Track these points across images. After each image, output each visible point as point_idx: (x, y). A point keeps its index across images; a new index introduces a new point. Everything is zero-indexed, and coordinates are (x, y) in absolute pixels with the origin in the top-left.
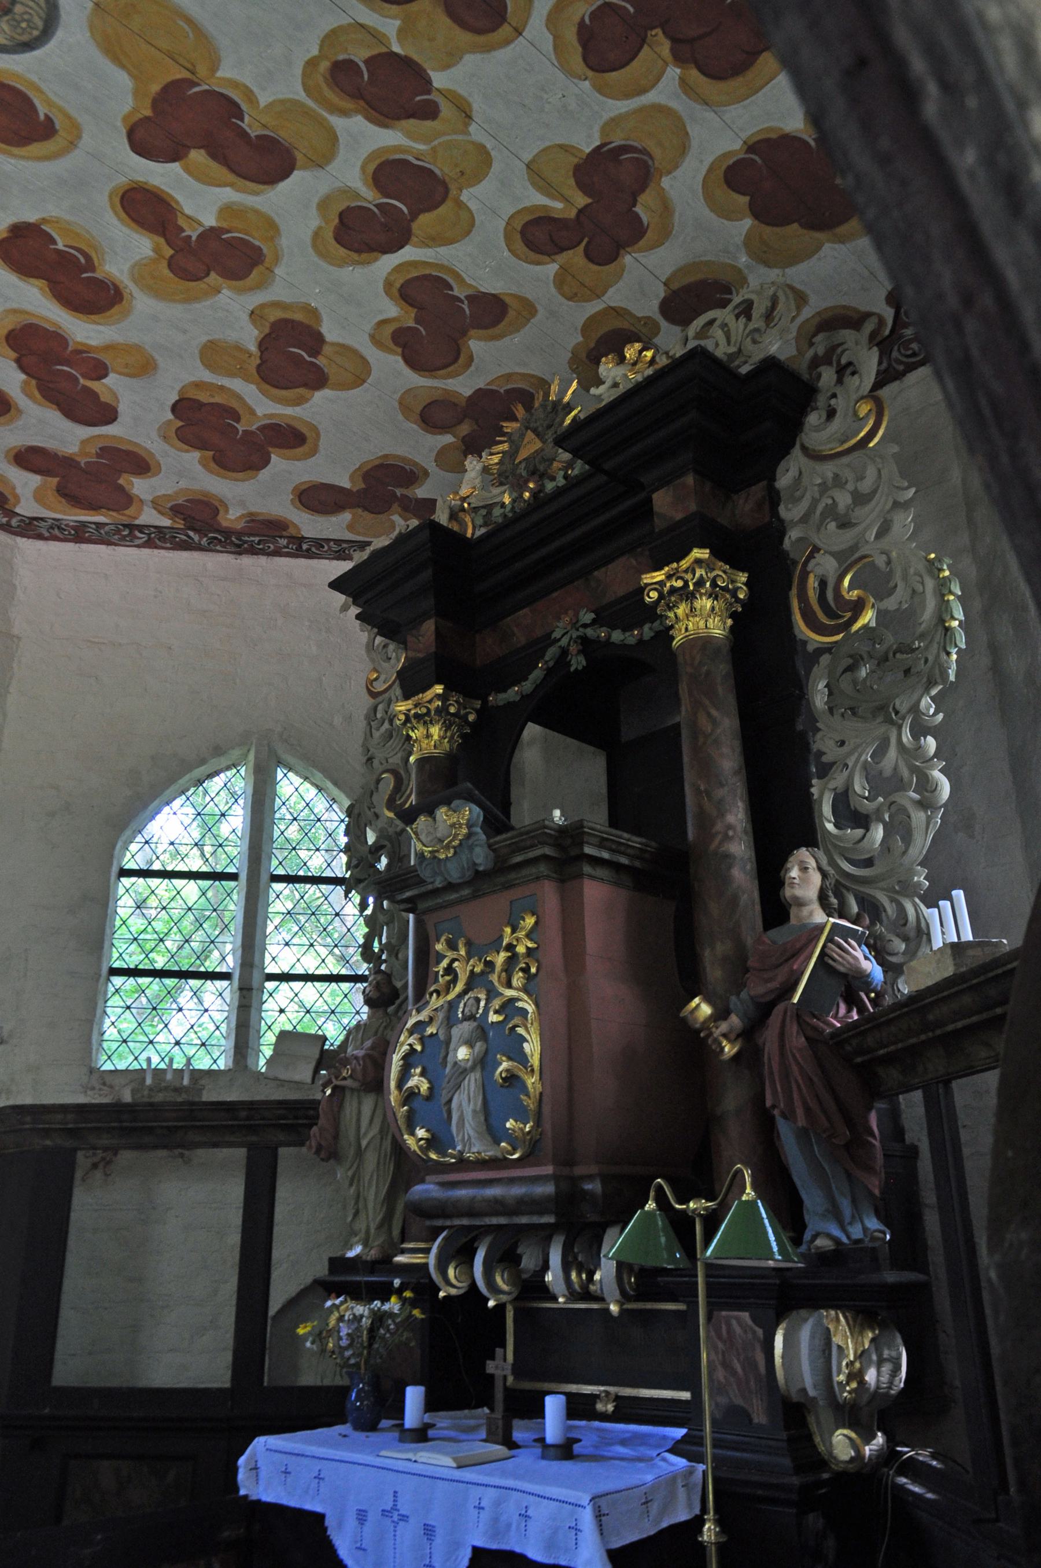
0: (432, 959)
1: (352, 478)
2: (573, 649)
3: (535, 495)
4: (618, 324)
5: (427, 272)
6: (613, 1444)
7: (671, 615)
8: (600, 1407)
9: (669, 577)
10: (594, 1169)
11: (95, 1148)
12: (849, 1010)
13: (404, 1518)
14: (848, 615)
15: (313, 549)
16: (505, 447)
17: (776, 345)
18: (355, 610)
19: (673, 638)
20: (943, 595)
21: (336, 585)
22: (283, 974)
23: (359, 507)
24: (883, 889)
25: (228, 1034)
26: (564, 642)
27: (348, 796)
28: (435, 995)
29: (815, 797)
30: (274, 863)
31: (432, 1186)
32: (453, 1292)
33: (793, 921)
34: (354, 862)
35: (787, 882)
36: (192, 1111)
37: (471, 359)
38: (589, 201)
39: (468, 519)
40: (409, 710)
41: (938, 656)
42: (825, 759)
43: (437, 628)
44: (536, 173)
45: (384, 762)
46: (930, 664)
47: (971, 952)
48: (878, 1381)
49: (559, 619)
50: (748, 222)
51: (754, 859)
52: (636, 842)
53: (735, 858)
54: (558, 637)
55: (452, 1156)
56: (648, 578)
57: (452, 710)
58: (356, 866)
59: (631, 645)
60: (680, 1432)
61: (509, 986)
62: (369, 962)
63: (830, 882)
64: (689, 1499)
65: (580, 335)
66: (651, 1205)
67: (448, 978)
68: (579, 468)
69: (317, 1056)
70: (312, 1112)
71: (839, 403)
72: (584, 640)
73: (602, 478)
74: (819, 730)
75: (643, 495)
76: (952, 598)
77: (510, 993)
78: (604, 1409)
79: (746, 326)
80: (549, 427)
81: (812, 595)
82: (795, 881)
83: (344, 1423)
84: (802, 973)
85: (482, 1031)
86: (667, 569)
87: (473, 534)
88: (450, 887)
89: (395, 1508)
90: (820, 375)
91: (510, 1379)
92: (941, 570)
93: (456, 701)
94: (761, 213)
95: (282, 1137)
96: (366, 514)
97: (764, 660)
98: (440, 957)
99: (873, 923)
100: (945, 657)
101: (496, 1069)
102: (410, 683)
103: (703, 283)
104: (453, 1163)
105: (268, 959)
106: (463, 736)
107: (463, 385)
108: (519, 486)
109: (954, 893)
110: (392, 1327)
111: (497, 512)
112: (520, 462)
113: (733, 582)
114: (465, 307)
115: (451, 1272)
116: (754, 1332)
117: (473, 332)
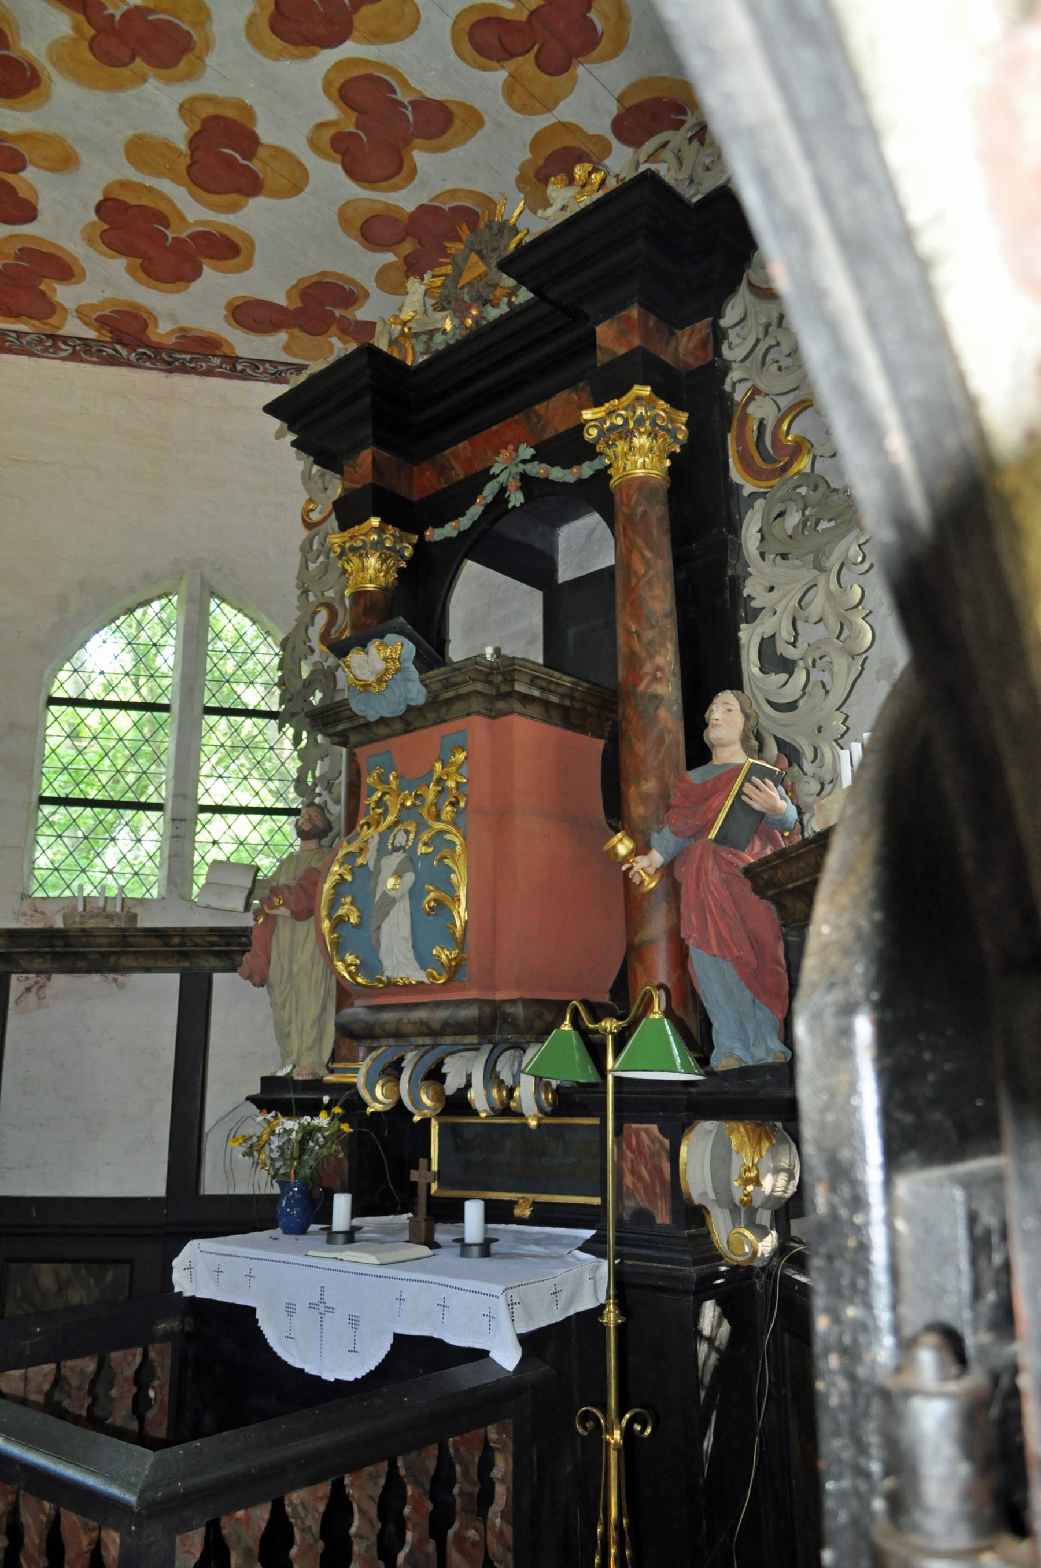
0: (364, 792)
1: (288, 295)
2: (513, 484)
3: (476, 321)
4: (568, 141)
8: (517, 1212)
9: (609, 414)
10: (516, 995)
12: (764, 847)
13: (330, 1310)
15: (248, 371)
16: (449, 269)
18: (291, 437)
19: (610, 477)
21: (273, 409)
31: (361, 1010)
32: (379, 1107)
33: (716, 761)
36: (125, 937)
37: (414, 171)
39: (408, 345)
40: (344, 543)
42: (754, 604)
43: (374, 458)
45: (319, 594)
49: (498, 454)
51: (680, 701)
52: (567, 681)
53: (662, 698)
54: (497, 472)
55: (380, 981)
56: (587, 415)
61: (438, 818)
63: (753, 722)
66: (566, 1027)
67: (379, 811)
68: (525, 295)
70: (244, 940)
72: (524, 477)
80: (494, 250)
82: (718, 722)
83: (275, 1227)
86: (607, 405)
87: (413, 361)
88: (382, 721)
93: (392, 535)
95: (214, 962)
96: (303, 335)
98: (372, 790)
102: (348, 512)
103: (657, 101)
106: (400, 571)
107: (406, 200)
108: (460, 313)
110: (321, 1139)
111: (439, 338)
112: (463, 287)
114: (409, 113)
115: (378, 1092)
116: (661, 1143)
117: (417, 142)
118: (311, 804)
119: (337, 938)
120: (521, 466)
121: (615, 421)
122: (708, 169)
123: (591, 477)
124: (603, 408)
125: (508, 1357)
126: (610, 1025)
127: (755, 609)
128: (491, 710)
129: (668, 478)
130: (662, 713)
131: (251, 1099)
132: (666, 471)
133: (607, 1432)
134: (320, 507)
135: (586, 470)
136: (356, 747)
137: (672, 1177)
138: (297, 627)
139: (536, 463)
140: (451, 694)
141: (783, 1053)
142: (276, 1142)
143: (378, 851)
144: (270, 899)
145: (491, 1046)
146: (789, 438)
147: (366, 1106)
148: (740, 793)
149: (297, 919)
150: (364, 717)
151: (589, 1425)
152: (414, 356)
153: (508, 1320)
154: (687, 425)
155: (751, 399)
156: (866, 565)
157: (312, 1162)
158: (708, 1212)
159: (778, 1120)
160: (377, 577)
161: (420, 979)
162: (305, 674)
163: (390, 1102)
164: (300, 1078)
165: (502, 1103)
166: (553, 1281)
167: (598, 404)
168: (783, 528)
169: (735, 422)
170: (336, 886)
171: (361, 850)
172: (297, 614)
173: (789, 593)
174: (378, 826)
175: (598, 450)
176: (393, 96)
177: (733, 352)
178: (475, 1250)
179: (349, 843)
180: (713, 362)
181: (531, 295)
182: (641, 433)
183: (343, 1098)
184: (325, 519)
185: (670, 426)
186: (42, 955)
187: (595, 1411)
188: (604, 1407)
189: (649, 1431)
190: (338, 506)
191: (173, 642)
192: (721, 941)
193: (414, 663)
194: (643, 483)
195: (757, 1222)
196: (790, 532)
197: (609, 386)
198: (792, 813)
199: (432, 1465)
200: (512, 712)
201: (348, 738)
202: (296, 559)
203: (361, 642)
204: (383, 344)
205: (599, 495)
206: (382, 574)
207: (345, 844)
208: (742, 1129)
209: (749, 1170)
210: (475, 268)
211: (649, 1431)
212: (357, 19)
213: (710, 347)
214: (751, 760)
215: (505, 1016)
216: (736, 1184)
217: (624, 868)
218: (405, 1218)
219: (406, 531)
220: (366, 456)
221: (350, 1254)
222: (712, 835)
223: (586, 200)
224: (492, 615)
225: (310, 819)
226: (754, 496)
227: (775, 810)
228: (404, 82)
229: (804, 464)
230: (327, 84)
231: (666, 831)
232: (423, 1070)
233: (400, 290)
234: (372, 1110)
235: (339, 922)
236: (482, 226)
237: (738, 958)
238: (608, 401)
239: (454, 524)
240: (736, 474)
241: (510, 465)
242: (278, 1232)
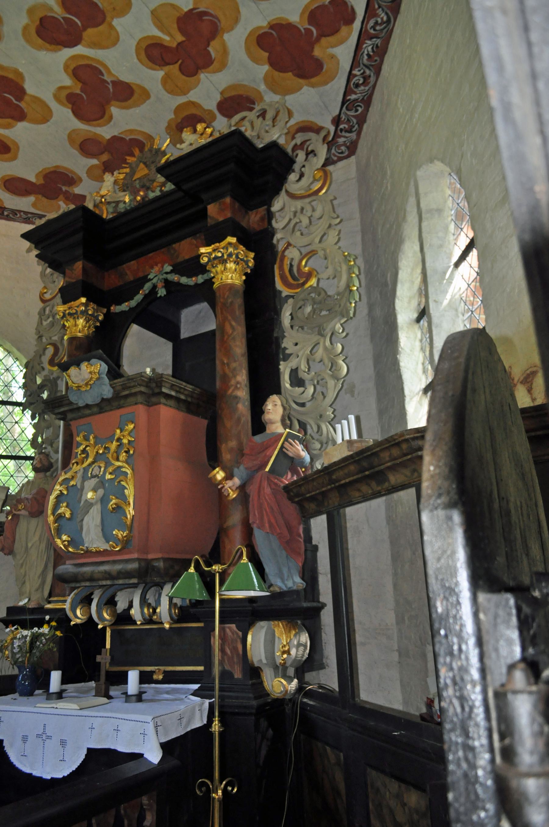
0: (74, 445)
1: (37, 176)
2: (160, 285)
3: (143, 198)
4: (194, 111)
5: (90, 62)
6: (161, 694)
7: (214, 270)
8: (155, 677)
9: (214, 250)
10: (159, 555)
12: (292, 476)
13: (49, 737)
15: (11, 215)
16: (127, 170)
17: (276, 135)
18: (36, 252)
19: (214, 283)
20: (351, 274)
21: (25, 236)
23: (40, 194)
26: (154, 281)
27: (25, 357)
28: (75, 464)
31: (70, 566)
32: (79, 621)
33: (268, 431)
34: (28, 393)
37: (111, 117)
38: (184, 39)
39: (104, 208)
40: (65, 311)
41: (345, 304)
42: (287, 352)
43: (83, 267)
44: (156, 16)
45: (49, 339)
46: (341, 307)
47: (356, 445)
48: (297, 653)
49: (152, 268)
50: (266, 67)
51: (249, 400)
52: (190, 388)
53: (240, 398)
54: (152, 278)
55: (82, 550)
56: (203, 250)
57: (90, 312)
58: (30, 396)
59: (191, 286)
60: (196, 686)
61: (118, 459)
62: (35, 449)
63: (287, 412)
64: (201, 717)
65: (173, 114)
66: (192, 570)
67: (83, 456)
68: (170, 187)
69: (4, 498)
71: (305, 170)
72: (166, 281)
73: (181, 194)
75: (201, 207)
76: (354, 275)
78: (157, 678)
79: (262, 123)
80: (153, 162)
81: (286, 268)
83: (14, 693)
84: (271, 457)
85: (102, 483)
86: (213, 246)
87: (107, 216)
88: (87, 406)
89: (44, 733)
90: (297, 155)
91: (108, 665)
92: (350, 261)
93: (92, 308)
94: (274, 63)
96: (44, 199)
97: (259, 299)
98: (79, 444)
100: (349, 305)
101: (109, 503)
102: (67, 295)
103: (240, 96)
104: (82, 554)
106: (96, 327)
107: (106, 132)
108: (134, 193)
109: (349, 416)
110: (44, 641)
111: (121, 206)
112: (135, 180)
113: (247, 257)
114: (110, 87)
115: (78, 612)
116: (237, 634)
117: (113, 102)
118: (41, 453)
122: (267, 132)
123: (203, 283)
124: (211, 247)
125: (154, 756)
126: (216, 568)
127: (288, 354)
128: (149, 402)
129: (244, 285)
130: (240, 406)
132: (242, 282)
133: (213, 793)
134: (50, 292)
135: (200, 279)
136: (71, 420)
138: (35, 356)
139: (173, 274)
141: (302, 584)
142: (17, 643)
143: (83, 477)
145: (144, 585)
146: (307, 269)
147: (70, 621)
148: (282, 447)
150: (77, 404)
151: (204, 789)
152: (106, 214)
153: (155, 735)
154: (254, 259)
155: (286, 248)
156: (344, 334)
157: (38, 654)
159: (299, 619)
160: (83, 330)
161: (105, 548)
163: (85, 618)
165: (150, 616)
166: (179, 712)
167: (208, 245)
168: (303, 314)
169: (278, 260)
170: (57, 497)
171: (73, 477)
176: (102, 77)
177: (277, 224)
178: (134, 698)
179: (66, 473)
180: (267, 229)
181: (173, 187)
182: (230, 261)
183: (57, 617)
185: (245, 259)
187: (206, 781)
188: (212, 780)
189: (236, 790)
190: (61, 290)
192: (271, 525)
193: (106, 375)
194: (231, 287)
195: (288, 675)
196: (306, 316)
197: (214, 236)
198: (308, 458)
199: (112, 821)
200: (160, 403)
201: (66, 416)
202: (36, 318)
204: (90, 206)
205: (207, 292)
206: (86, 329)
207: (63, 473)
208: (280, 624)
209: (284, 646)
210: (142, 171)
211: (236, 790)
212: (85, 35)
213: (266, 221)
215: (154, 567)
217: (219, 487)
218: (93, 684)
220: (79, 265)
221: (61, 705)
222: (267, 469)
223: (203, 141)
224: (145, 353)
226: (288, 297)
228: (109, 72)
229: (313, 282)
230: (66, 67)
231: (242, 467)
232: (104, 600)
233: (101, 180)
234: (74, 623)
235: (59, 518)
236: (146, 149)
238: (214, 244)
239: (127, 304)
240: (279, 285)
241: (159, 274)
242: (16, 695)
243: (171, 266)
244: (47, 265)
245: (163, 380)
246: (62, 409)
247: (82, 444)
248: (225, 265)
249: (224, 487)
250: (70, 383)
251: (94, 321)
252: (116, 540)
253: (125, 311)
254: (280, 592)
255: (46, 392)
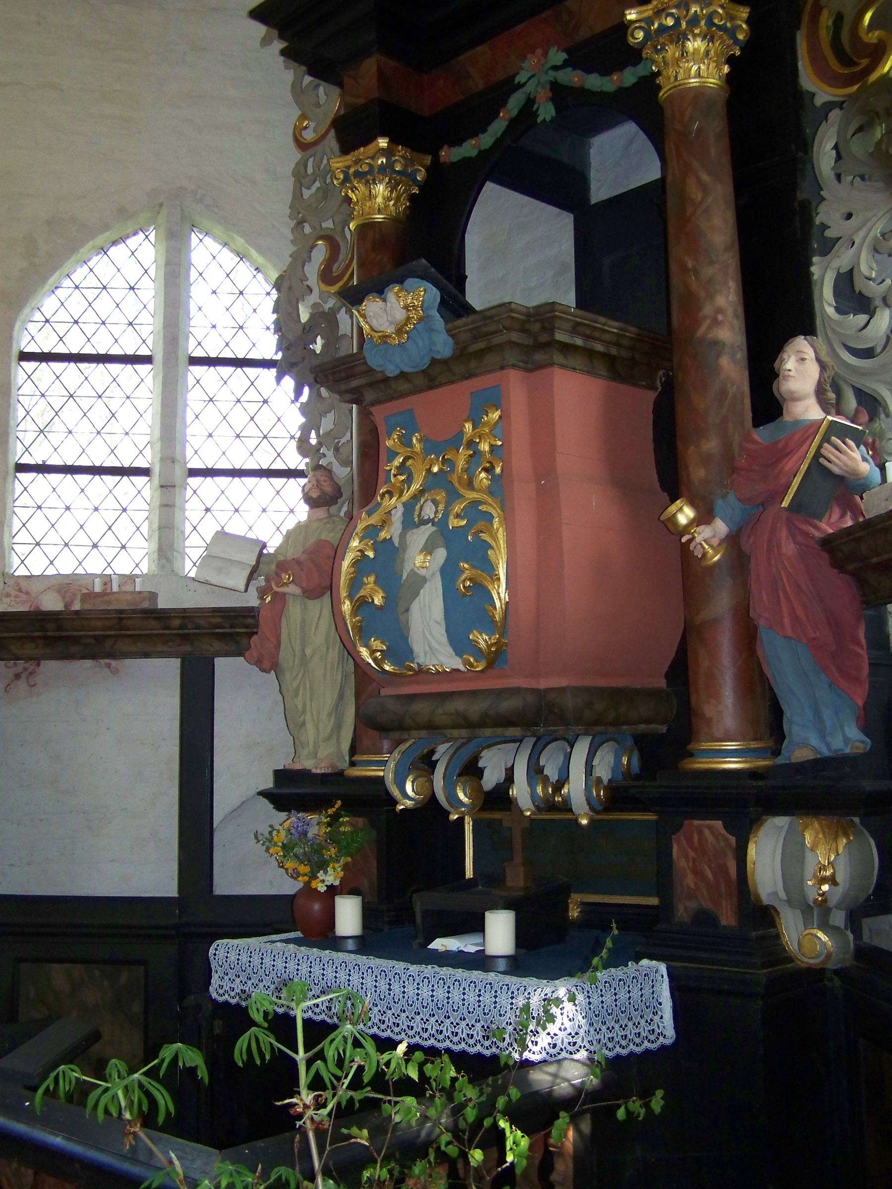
7: (658, 58)
10: (563, 682)
11: (17, 658)
14: (865, 62)
19: (659, 88)
22: (207, 469)
24: (885, 382)
25: (150, 536)
26: (530, 87)
29: (815, 277)
30: (192, 343)
32: (409, 803)
33: (787, 417)
35: (781, 374)
36: (121, 619)
40: (348, 167)
42: (828, 233)
43: (379, 69)
49: (524, 58)
51: (745, 347)
52: (613, 326)
53: (724, 344)
54: (523, 81)
61: (470, 485)
63: (829, 374)
67: (402, 478)
70: (250, 621)
74: (823, 199)
77: (473, 495)
81: (825, 36)
82: (791, 373)
88: (403, 375)
93: (402, 157)
95: (217, 645)
99: (871, 419)
102: (351, 132)
105: (189, 452)
106: (412, 198)
113: (732, 18)
116: (727, 840)
118: (317, 467)
119: (360, 621)
120: (552, 73)
121: (664, 22)
123: (634, 85)
124: (650, 6)
131: (263, 794)
134: (312, 125)
135: (629, 77)
136: (372, 405)
137: (738, 875)
139: (569, 69)
140: (482, 345)
141: (863, 742)
144: (278, 575)
148: (818, 454)
149: (309, 598)
150: (382, 372)
154: (748, 22)
158: (778, 913)
159: (855, 815)
160: (387, 206)
162: (304, 317)
164: (318, 771)
172: (292, 249)
173: (869, 220)
174: (401, 496)
175: (644, 56)
179: (369, 514)
182: (695, 36)
184: (323, 137)
186: (33, 639)
191: (151, 285)
194: (699, 93)
200: (552, 364)
203: (376, 286)
205: (645, 105)
206: (392, 203)
209: (824, 868)
214: (830, 418)
216: (810, 883)
217: (684, 540)
219: (418, 151)
220: (370, 66)
222: (785, 504)
224: (517, 251)
225: (318, 485)
226: (829, 106)
227: (855, 473)
231: (731, 497)
234: (402, 807)
235: (361, 605)
237: (814, 639)
240: (808, 80)
241: (538, 71)
243: (563, 51)
244: (304, 68)
245: (555, 317)
246: (354, 383)
247: (398, 454)
248: (683, 46)
249: (693, 538)
250: (366, 327)
251: (406, 185)
252: (478, 652)
253: (470, 158)
254: (816, 762)
255: (319, 340)
